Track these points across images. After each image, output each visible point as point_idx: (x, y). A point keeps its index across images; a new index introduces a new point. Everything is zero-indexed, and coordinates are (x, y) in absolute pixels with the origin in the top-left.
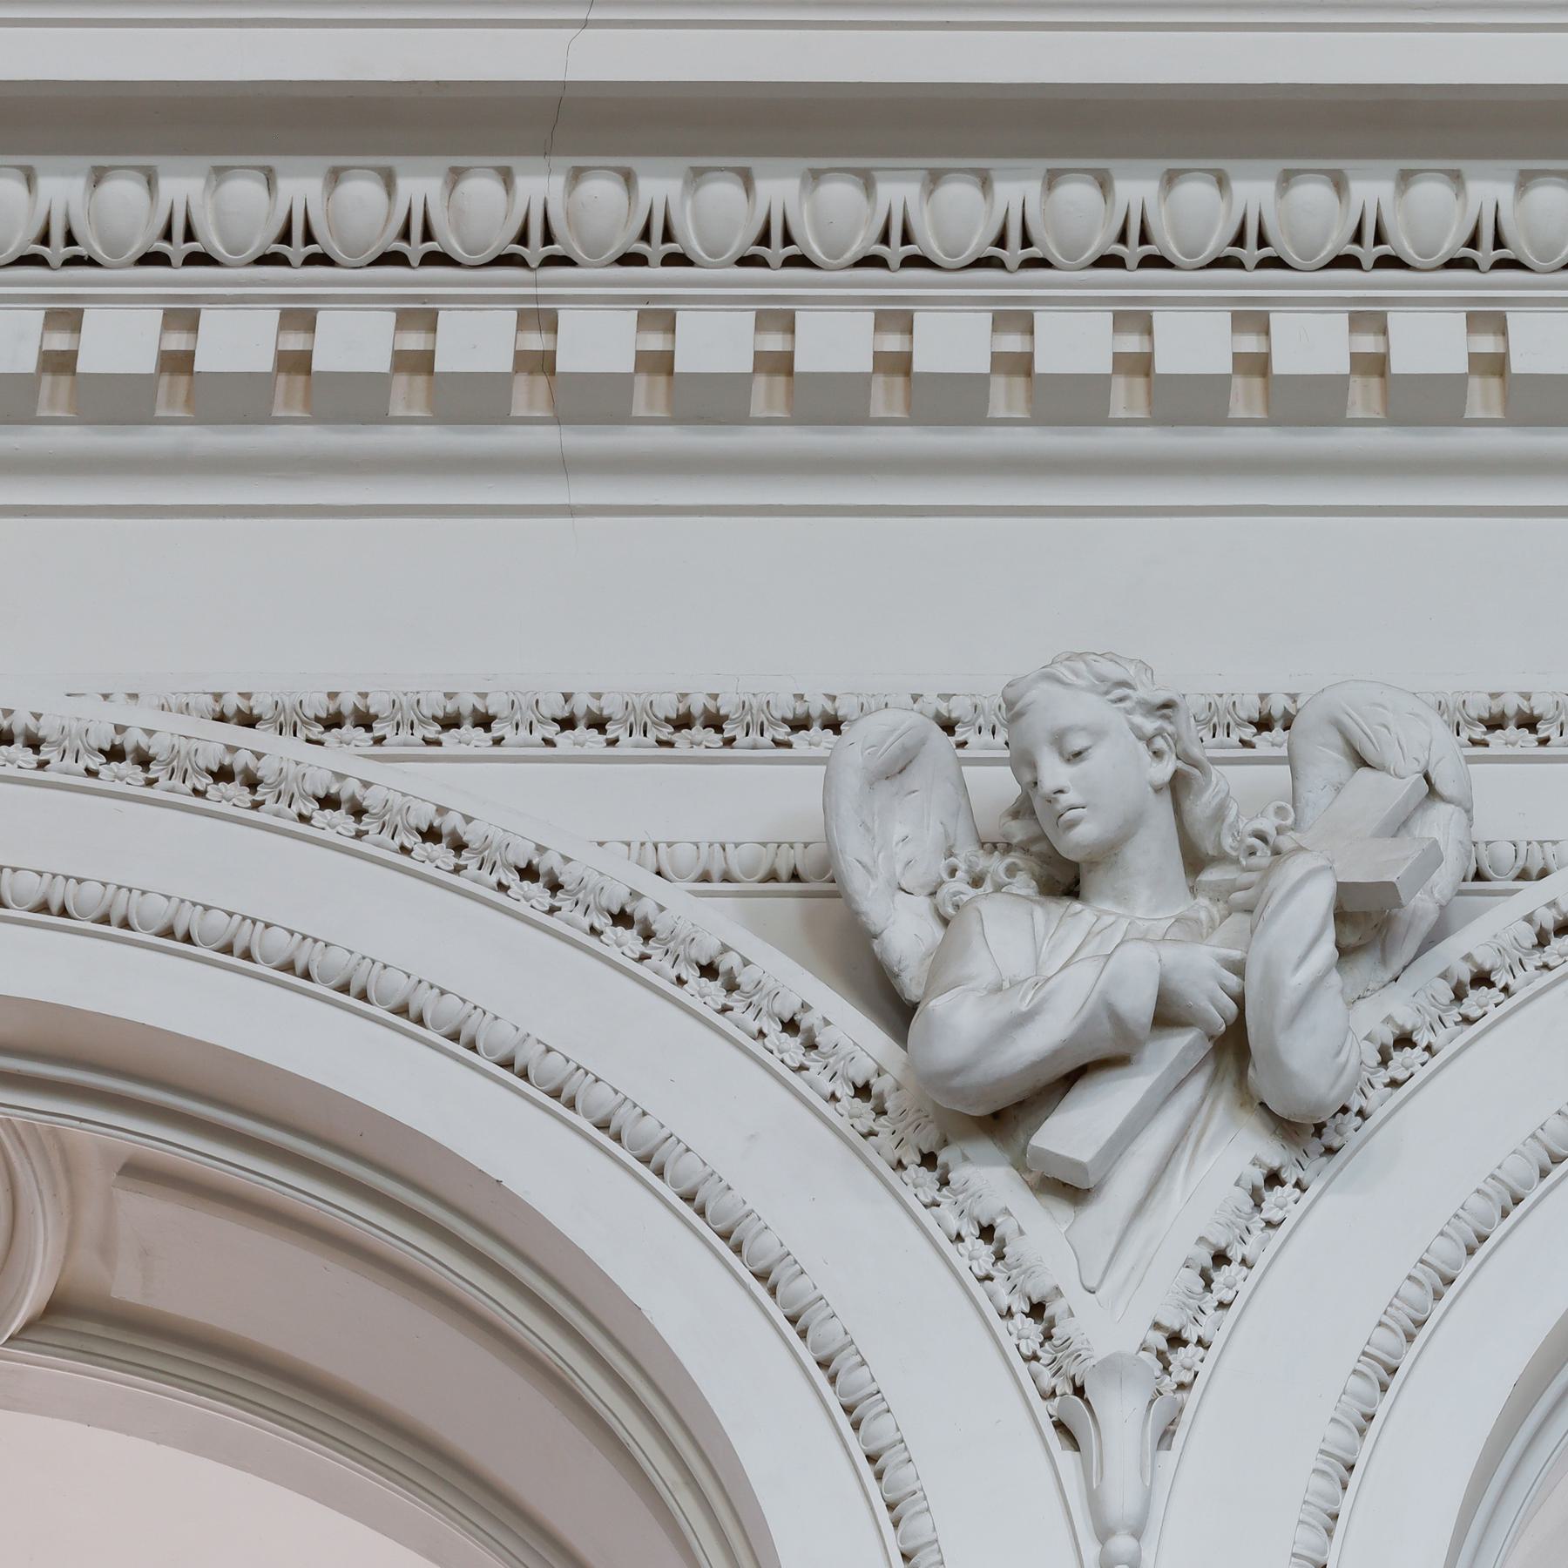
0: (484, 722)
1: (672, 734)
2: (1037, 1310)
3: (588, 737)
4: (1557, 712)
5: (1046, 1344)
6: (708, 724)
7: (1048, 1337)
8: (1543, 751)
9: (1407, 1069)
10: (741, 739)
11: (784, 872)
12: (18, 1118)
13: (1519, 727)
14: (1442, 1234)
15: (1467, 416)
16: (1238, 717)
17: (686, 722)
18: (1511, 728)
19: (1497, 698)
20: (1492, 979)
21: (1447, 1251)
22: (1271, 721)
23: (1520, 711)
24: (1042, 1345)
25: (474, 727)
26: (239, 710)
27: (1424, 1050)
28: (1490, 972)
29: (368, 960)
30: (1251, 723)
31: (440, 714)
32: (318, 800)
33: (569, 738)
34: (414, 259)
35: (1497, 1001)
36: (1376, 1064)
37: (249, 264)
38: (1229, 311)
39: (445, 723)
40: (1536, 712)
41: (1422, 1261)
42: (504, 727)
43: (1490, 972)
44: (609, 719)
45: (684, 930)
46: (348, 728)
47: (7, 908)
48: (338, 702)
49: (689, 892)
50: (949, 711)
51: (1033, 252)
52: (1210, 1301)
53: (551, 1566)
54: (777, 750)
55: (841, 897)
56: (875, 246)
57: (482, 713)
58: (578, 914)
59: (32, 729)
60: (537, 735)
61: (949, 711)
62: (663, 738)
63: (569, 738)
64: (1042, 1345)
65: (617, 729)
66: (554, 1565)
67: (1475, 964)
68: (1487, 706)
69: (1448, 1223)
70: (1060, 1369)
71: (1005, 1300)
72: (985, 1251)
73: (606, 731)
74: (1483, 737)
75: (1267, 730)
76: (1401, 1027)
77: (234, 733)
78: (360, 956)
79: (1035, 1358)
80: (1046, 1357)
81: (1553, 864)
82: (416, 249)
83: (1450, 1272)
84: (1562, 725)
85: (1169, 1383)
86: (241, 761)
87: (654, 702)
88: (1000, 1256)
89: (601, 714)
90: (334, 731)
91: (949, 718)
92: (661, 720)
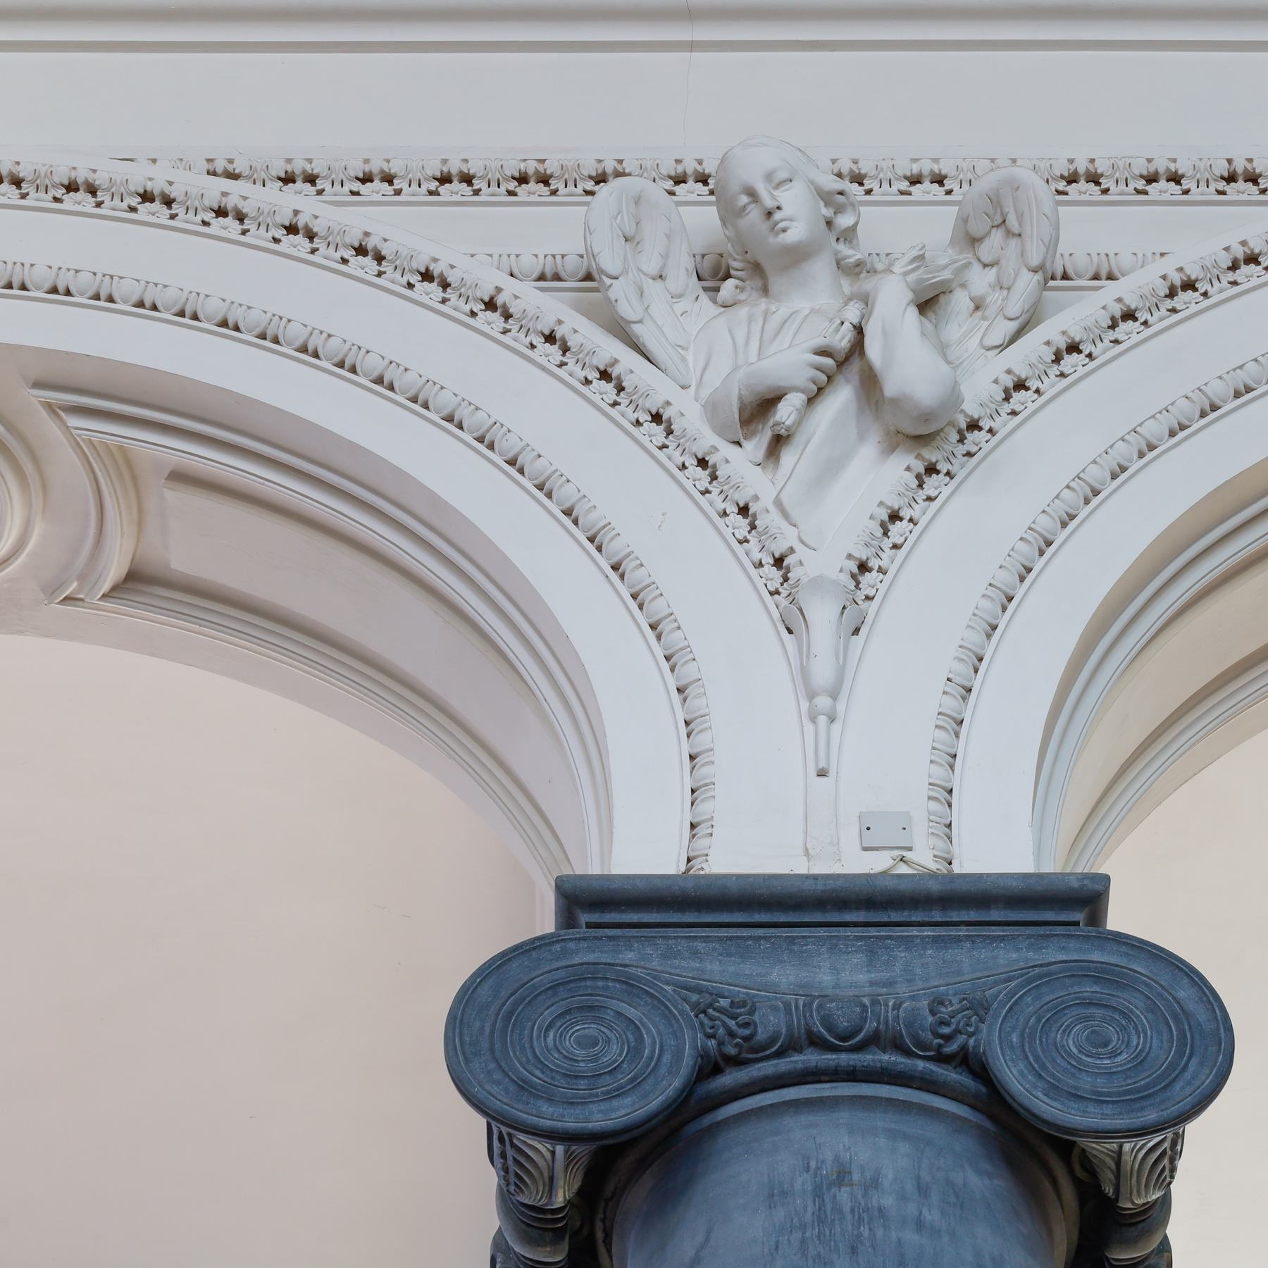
0: (1176, 178)
1: (1066, 186)
2: (779, 562)
3: (382, 187)
5: (785, 584)
6: (1169, 178)
7: (786, 579)
8: (1105, 198)
9: (1023, 404)
10: (562, 190)
12: (96, 438)
13: (1168, 181)
14: (1044, 511)
17: (603, 179)
18: (1082, 182)
20: (1081, 348)
21: (1045, 524)
22: (372, 177)
23: (852, 171)
24: (782, 584)
25: (932, 183)
26: (537, 171)
27: (1035, 392)
28: (1079, 343)
30: (435, 179)
31: (1145, 173)
32: (286, 228)
33: (683, 189)
35: (1084, 363)
36: (1001, 400)
40: (1257, 171)
41: (1030, 529)
43: (1079, 343)
44: (318, 177)
45: (531, 312)
46: (691, 183)
47: (115, 303)
50: (469, 170)
52: (887, 543)
55: (600, 292)
57: (542, 173)
58: (461, 303)
59: (91, 181)
60: (347, 188)
61: (859, 169)
62: (588, 188)
63: (683, 189)
64: (782, 584)
65: (401, 183)
67: (1069, 337)
69: (1048, 506)
70: (793, 600)
71: (757, 556)
72: (743, 523)
74: (1144, 188)
75: (526, 183)
76: (1019, 377)
77: (228, 184)
79: (777, 592)
80: (784, 593)
83: (1050, 537)
84: (961, 181)
85: (860, 596)
86: (230, 203)
88: (753, 527)
89: (860, 173)
90: (1074, 185)
91: (468, 173)
92: (509, 177)
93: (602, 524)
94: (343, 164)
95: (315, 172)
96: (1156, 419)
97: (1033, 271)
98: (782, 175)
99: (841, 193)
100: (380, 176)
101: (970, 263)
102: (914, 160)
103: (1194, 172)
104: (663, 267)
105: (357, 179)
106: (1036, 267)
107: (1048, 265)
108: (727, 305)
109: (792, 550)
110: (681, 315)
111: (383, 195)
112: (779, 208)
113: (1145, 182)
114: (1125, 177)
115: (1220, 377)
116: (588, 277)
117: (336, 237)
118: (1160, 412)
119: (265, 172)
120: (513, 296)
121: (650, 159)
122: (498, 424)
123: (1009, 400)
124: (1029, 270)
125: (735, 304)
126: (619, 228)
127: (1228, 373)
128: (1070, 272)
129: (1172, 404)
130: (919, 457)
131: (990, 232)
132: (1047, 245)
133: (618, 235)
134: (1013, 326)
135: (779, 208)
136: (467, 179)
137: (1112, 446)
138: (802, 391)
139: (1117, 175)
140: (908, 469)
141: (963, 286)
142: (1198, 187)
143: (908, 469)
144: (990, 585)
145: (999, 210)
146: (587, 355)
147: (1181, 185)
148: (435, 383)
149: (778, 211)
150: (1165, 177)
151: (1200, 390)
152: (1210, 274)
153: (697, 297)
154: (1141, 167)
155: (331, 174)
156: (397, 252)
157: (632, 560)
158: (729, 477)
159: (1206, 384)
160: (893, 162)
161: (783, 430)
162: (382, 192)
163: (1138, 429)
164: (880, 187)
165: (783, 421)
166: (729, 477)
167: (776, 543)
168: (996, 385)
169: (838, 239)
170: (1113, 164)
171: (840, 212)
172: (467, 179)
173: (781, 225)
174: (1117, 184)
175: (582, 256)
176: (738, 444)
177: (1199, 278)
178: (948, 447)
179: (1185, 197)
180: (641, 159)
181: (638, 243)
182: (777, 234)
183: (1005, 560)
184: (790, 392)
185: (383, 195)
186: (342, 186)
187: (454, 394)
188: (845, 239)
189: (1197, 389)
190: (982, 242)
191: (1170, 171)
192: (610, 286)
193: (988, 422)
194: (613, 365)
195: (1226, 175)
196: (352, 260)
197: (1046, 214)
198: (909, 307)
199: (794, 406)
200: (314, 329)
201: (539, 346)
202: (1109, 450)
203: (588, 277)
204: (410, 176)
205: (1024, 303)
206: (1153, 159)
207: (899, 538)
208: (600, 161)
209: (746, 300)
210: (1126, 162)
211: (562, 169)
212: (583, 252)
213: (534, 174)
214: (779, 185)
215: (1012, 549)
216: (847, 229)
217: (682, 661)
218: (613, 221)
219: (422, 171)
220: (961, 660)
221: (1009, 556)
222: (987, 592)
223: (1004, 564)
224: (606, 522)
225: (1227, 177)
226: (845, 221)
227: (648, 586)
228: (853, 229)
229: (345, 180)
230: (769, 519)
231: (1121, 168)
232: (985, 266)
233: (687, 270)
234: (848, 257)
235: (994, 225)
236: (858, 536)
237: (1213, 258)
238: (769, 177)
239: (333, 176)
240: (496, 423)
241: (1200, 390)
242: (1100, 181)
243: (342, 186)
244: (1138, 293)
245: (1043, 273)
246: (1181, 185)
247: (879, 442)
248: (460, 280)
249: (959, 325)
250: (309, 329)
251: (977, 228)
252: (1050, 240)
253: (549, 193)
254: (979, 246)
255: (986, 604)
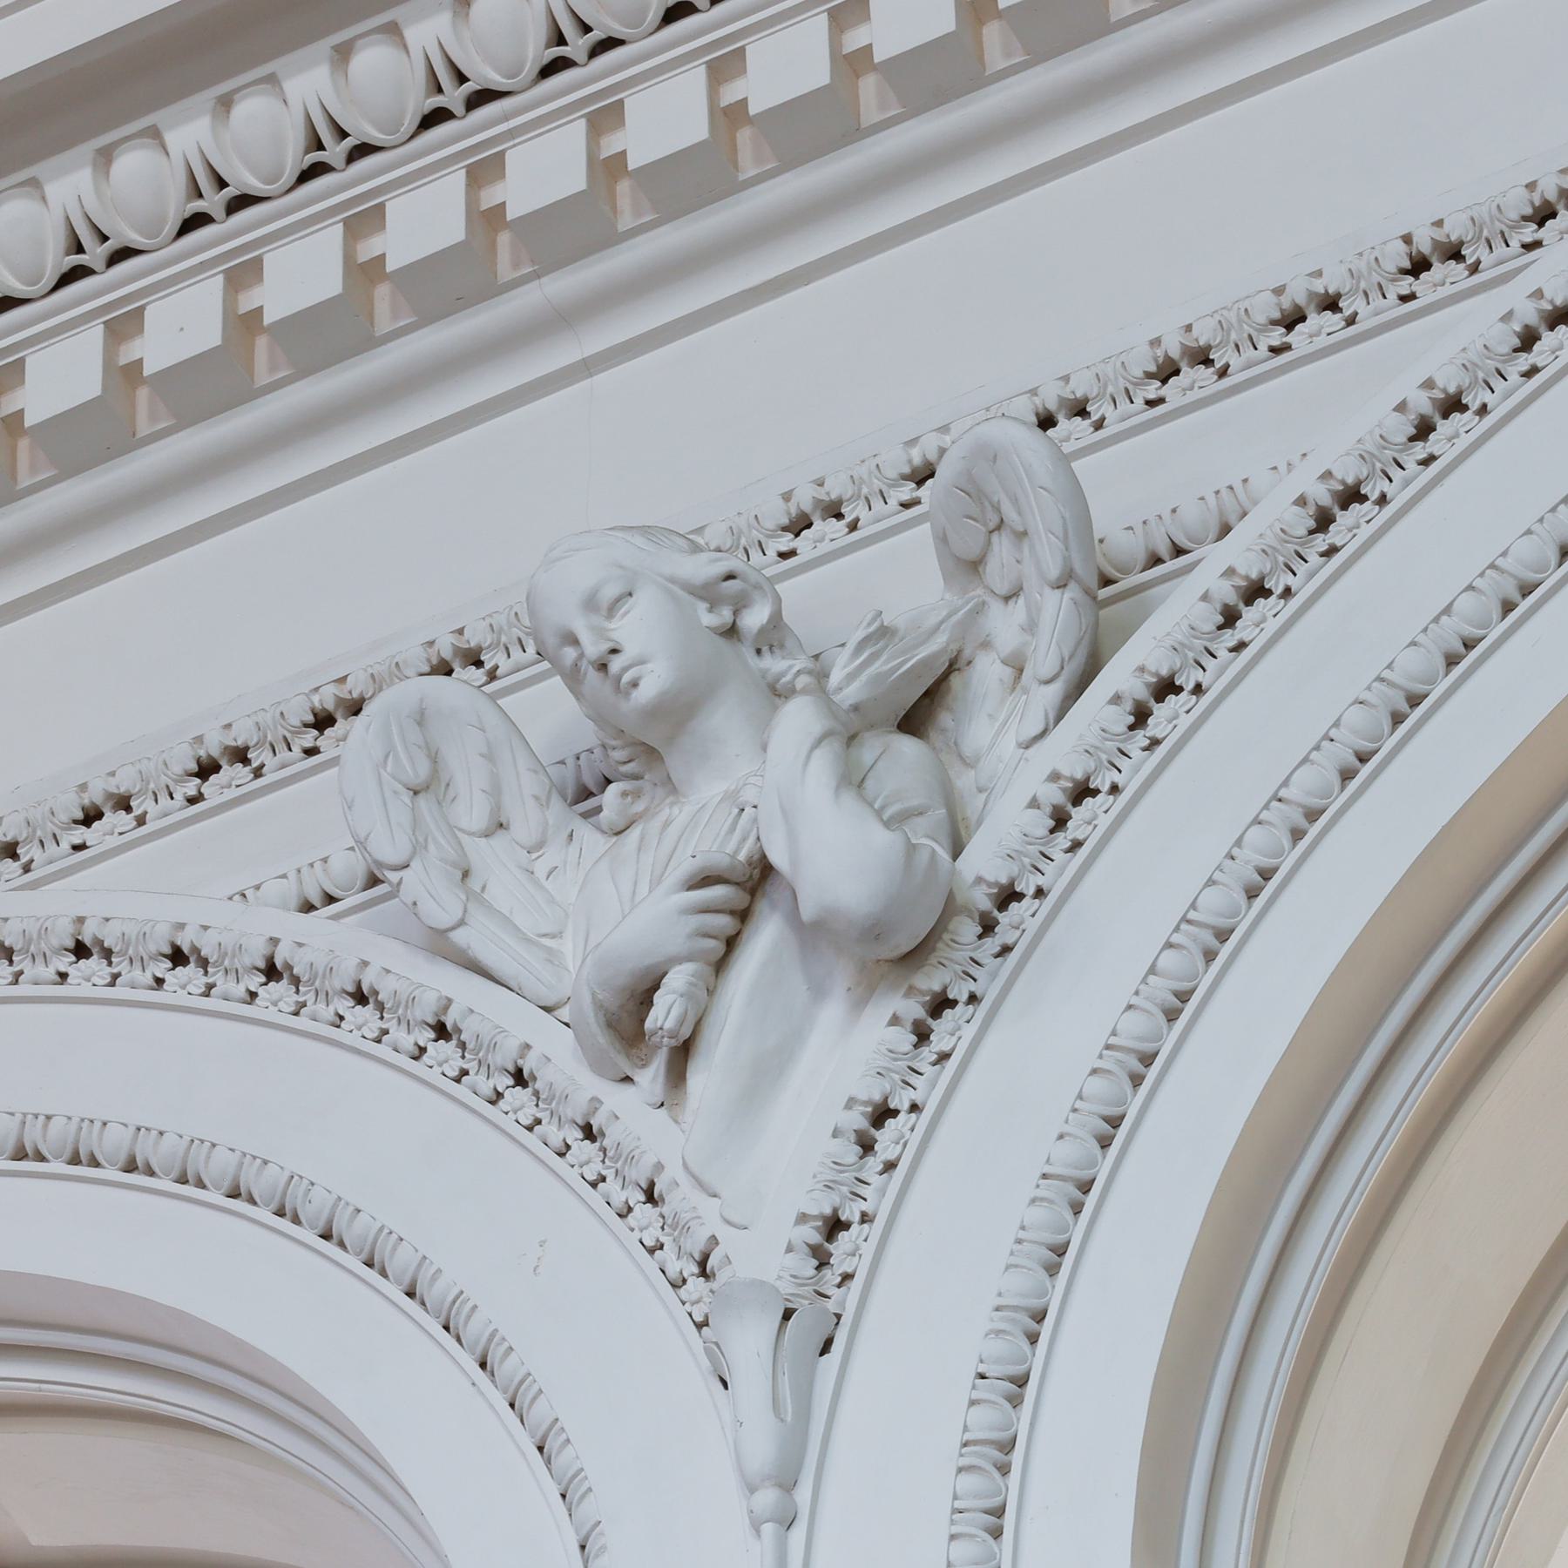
4: (30, 830)
10: (1486, 258)
11: (1163, 550)
15: (1113, 19)
16: (1386, 272)
19: (917, 442)
20: (1177, 683)
29: (86, 1122)
34: (458, 109)
37: (659, 28)
38: (823, 12)
39: (1288, 322)
42: (1101, 406)
44: (1461, 243)
46: (818, 525)
48: (1539, 189)
49: (329, 918)
51: (597, 35)
53: (1566, 1315)
54: (1279, 357)
56: (306, 157)
57: (349, 700)
60: (65, 846)
62: (1528, 239)
66: (1565, 1311)
68: (424, 660)
73: (1089, 413)
78: (79, 1119)
81: (1232, 519)
82: (453, 97)
87: (1501, 205)
93: (450, 1298)
94: (47, 809)
95: (833, 497)
96: (1313, 763)
97: (1058, 588)
98: (610, 592)
99: (730, 577)
100: (110, 804)
101: (984, 603)
102: (912, 442)
103: (495, 636)
104: (497, 808)
105: (76, 822)
106: (1058, 579)
107: (1079, 568)
108: (618, 830)
109: (714, 1241)
110: (547, 878)
111: (121, 834)
112: (614, 651)
113: (1284, 330)
114: (1246, 335)
115: (1413, 644)
116: (373, 881)
117: (39, 943)
118: (1317, 748)
119: (757, 530)
120: (295, 945)
121: (504, 610)
122: (296, 1178)
123: (829, 1263)
124: (1053, 588)
125: (632, 824)
126: (394, 778)
127: (1425, 630)
128: (1183, 542)
129: (1336, 724)
130: (911, 991)
131: (989, 543)
132: (1061, 535)
133: (395, 792)
134: (1055, 691)
135: (614, 651)
136: (240, 755)
137: (1238, 843)
138: (689, 958)
139: (1233, 336)
140: (895, 1021)
141: (986, 645)
142: (1368, 303)
143: (895, 1021)
144: (1044, 1176)
145: (987, 504)
146: (407, 1007)
147: (1341, 310)
148: (202, 1141)
149: (613, 657)
150: (1312, 307)
151: (1382, 680)
152: (1380, 461)
153: (571, 835)
154: (1267, 308)
155: (34, 831)
156: (123, 934)
157: (498, 1344)
158: (619, 1144)
159: (1389, 666)
160: (877, 460)
161: (666, 1039)
162: (117, 830)
163: (1283, 793)
164: (870, 509)
165: (659, 1025)
166: (619, 1144)
167: (691, 1237)
168: (1036, 811)
169: (759, 651)
170: (1220, 322)
171: (745, 607)
172: (240, 755)
173: (626, 678)
174: (1239, 351)
175: (352, 849)
176: (627, 1079)
177: (1362, 478)
178: (962, 955)
179: (1352, 330)
180: (490, 616)
181: (448, 785)
182: (627, 695)
183: (1067, 1122)
184: (670, 968)
185: (121, 834)
186: (58, 845)
187: (230, 1149)
188: (771, 647)
189: (1375, 680)
190: (986, 564)
191: (1317, 294)
192: (399, 883)
193: (1031, 879)
194: (446, 1008)
195: (1407, 264)
196: (71, 971)
197: (1045, 486)
198: (817, 753)
199: (674, 992)
200: (25, 1115)
201: (347, 1015)
202: (1235, 852)
203: (373, 881)
204: (152, 786)
205: (1059, 647)
206: (1284, 285)
207: (894, 1148)
208: (431, 643)
209: (647, 810)
210: (1239, 309)
211: (1099, 380)
212: (353, 844)
213: (1182, 357)
214: (612, 609)
215: (1080, 1097)
216: (762, 631)
217: (576, 1498)
218: (382, 771)
219: (165, 770)
220: (998, 1332)
221: (1075, 1110)
222: (1040, 1193)
223: (1067, 1129)
224: (455, 1292)
225: (1410, 267)
226: (755, 618)
227: (522, 1382)
228: (776, 621)
229: (58, 832)
230: (680, 1197)
231: (1235, 325)
232: (1007, 599)
233: (537, 798)
234: (783, 674)
235: (991, 529)
236: (814, 1176)
237: (1377, 432)
238: (590, 604)
239: (39, 833)
240: (292, 1177)
241: (1382, 680)
242: (1211, 357)
243: (58, 845)
244: (1256, 548)
245: (1076, 581)
246: (1341, 310)
247: (849, 989)
248: (217, 947)
249: (990, 716)
250: (19, 1117)
251: (969, 546)
252: (1065, 524)
253: (1343, 323)
254: (985, 569)
255: (1038, 1214)
